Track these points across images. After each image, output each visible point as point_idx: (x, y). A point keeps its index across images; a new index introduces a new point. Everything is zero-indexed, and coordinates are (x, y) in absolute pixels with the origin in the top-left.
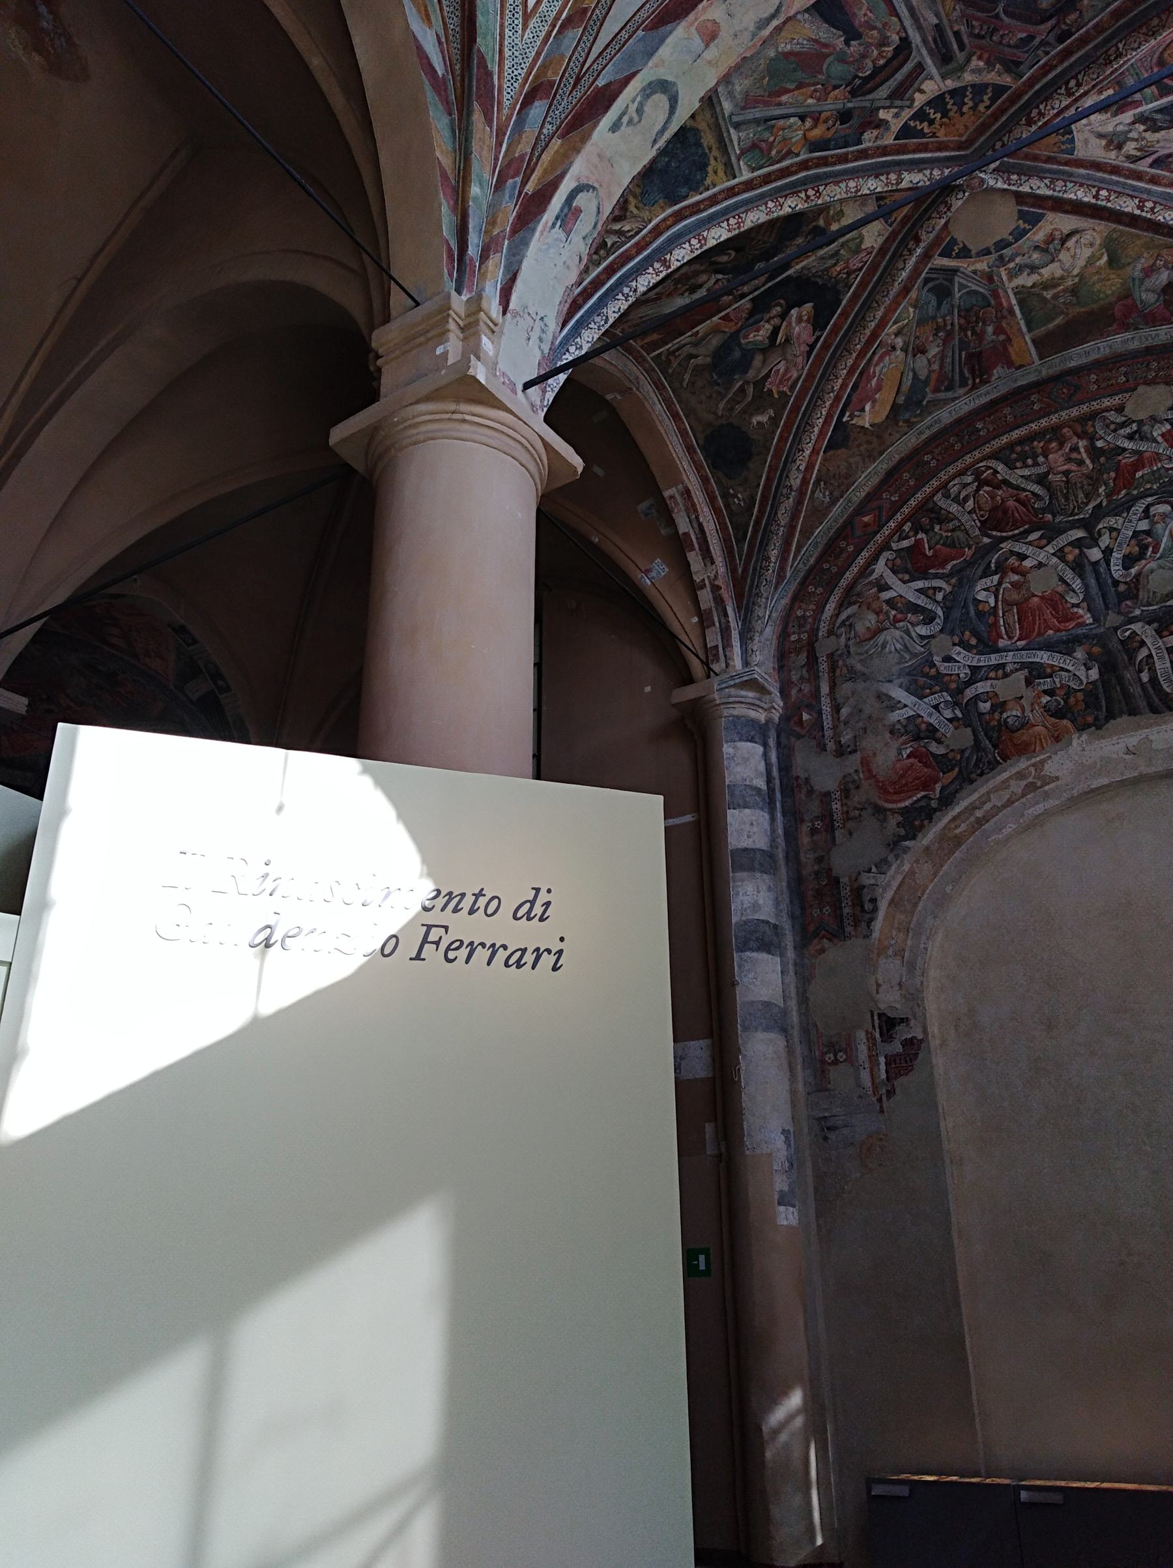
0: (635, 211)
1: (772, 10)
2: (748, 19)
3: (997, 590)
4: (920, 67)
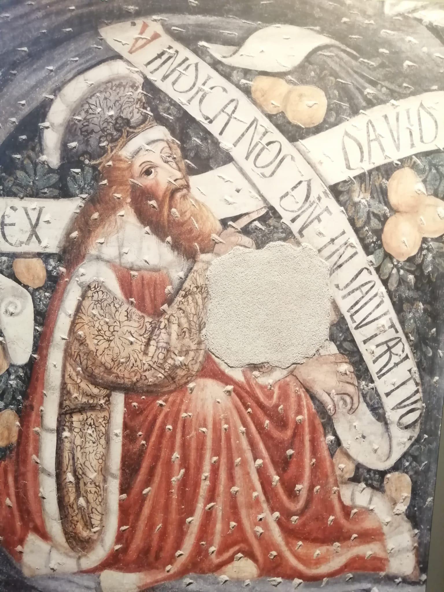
3: (54, 283)
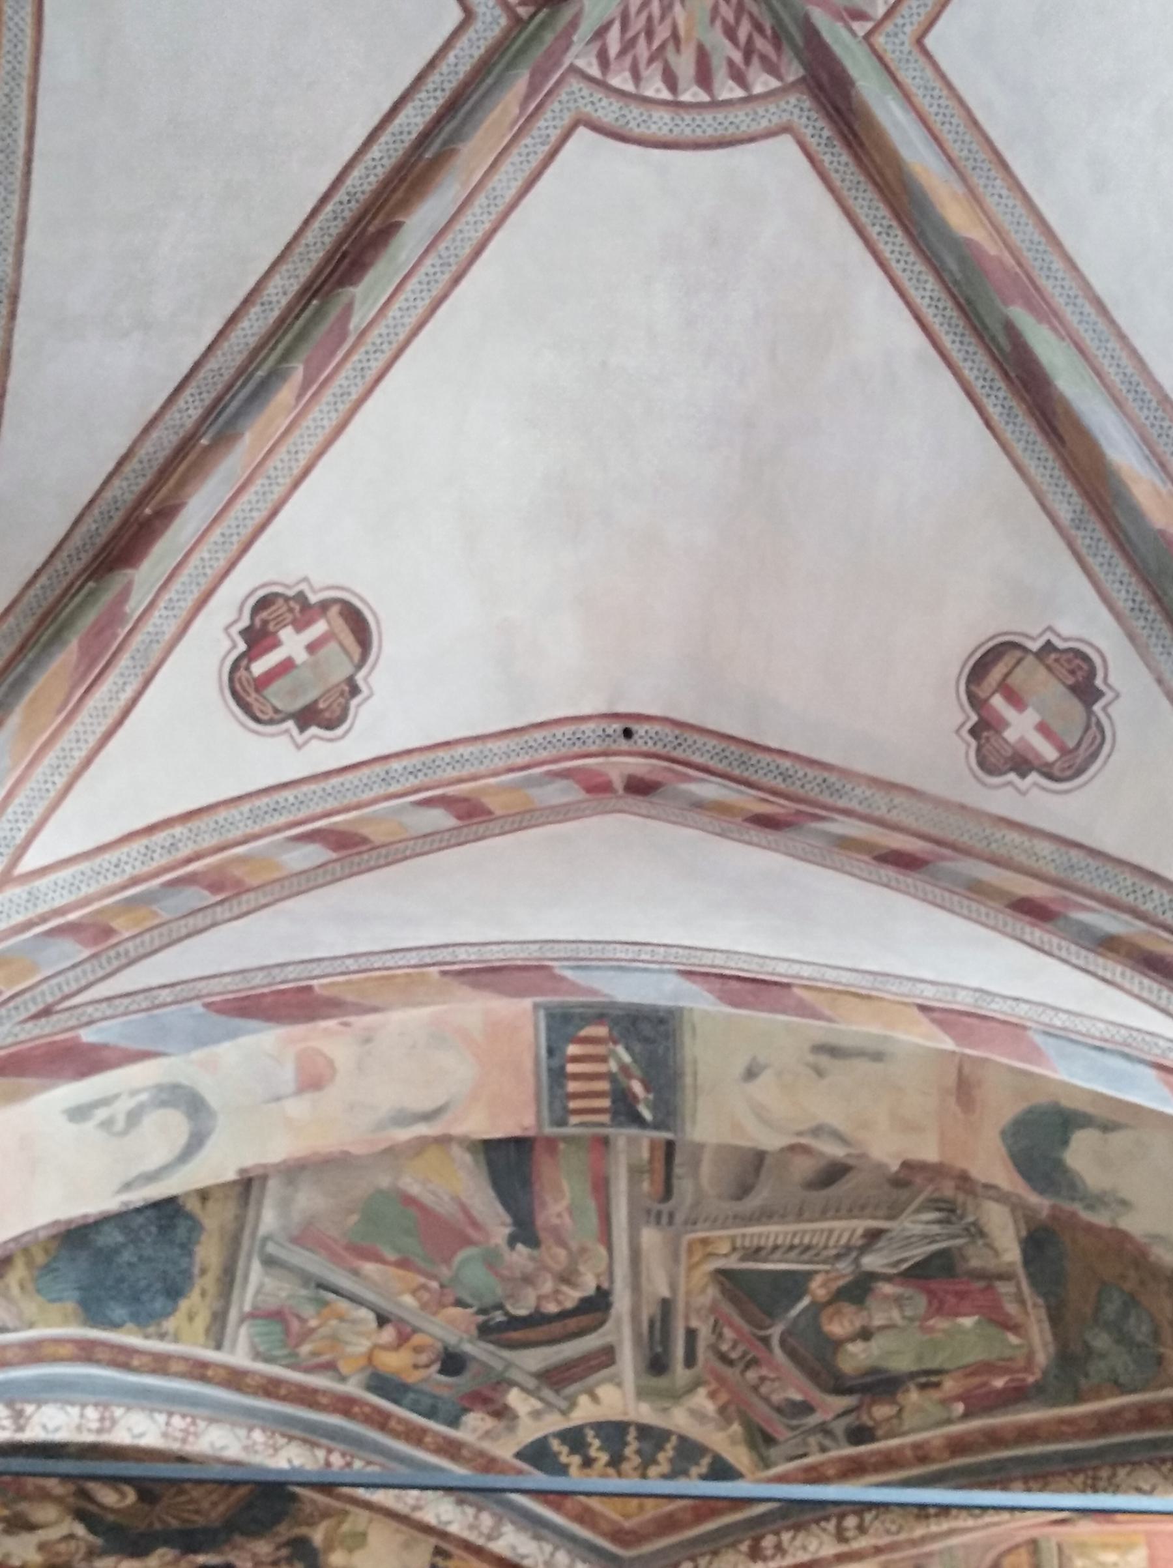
0: (15, 1290)
1: (428, 1105)
2: (388, 1095)
4: (607, 1356)
